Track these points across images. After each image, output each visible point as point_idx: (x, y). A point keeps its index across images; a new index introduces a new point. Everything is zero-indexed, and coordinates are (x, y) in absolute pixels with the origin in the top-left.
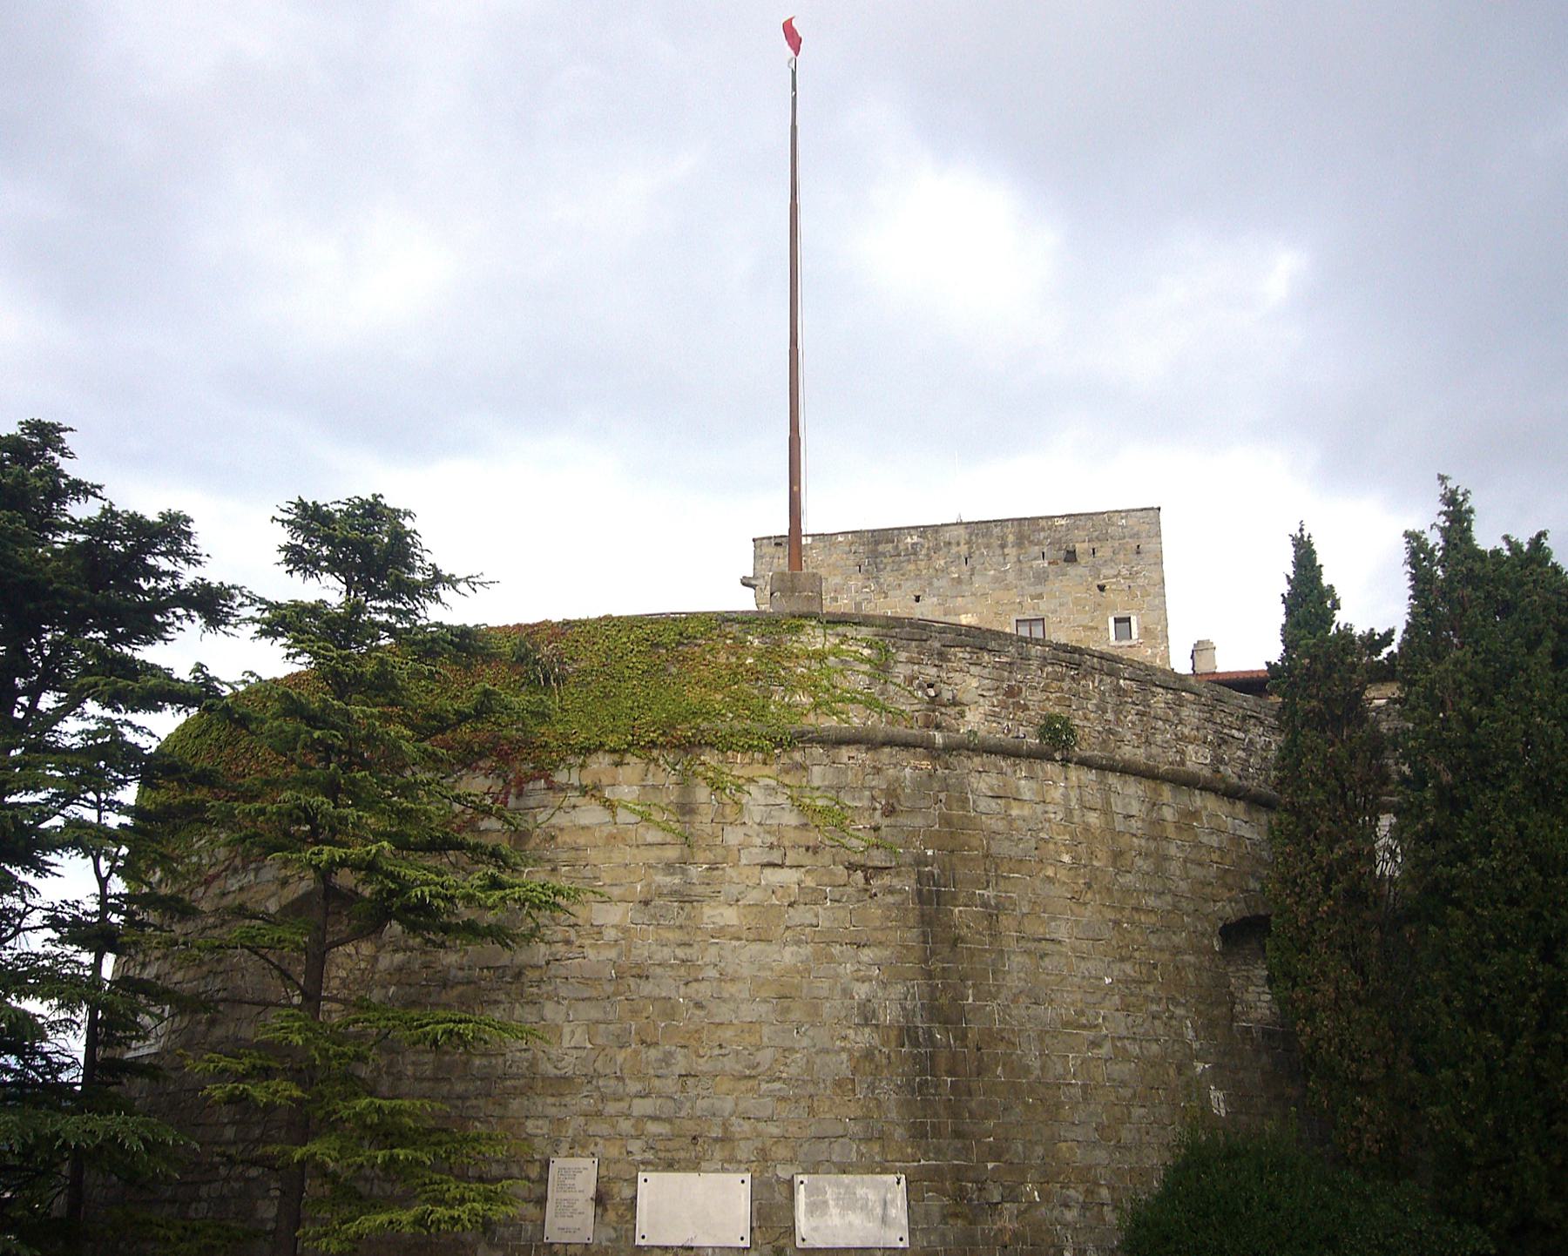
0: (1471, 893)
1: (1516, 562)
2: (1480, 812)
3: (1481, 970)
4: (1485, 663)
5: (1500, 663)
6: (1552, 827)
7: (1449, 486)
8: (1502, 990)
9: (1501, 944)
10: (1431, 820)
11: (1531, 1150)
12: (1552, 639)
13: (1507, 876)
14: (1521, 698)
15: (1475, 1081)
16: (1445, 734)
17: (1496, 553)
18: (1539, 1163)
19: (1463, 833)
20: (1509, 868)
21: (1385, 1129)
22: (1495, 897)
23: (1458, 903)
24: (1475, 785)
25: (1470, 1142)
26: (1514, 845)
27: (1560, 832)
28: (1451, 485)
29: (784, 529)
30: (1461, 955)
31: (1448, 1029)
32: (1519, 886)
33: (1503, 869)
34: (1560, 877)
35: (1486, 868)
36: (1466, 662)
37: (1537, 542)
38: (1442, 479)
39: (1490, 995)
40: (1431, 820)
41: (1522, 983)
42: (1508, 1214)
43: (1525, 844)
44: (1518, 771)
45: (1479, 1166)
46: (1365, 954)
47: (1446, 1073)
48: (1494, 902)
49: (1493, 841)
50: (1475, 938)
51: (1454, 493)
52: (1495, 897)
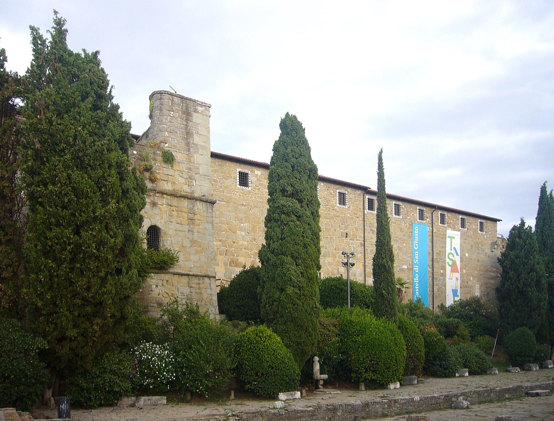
0: (46, 201)
1: (85, 61)
2: (53, 165)
3: (49, 234)
4: (62, 99)
5: (69, 101)
6: (83, 178)
7: (58, 16)
8: (57, 244)
9: (58, 225)
10: (30, 164)
11: (65, 309)
12: (93, 97)
13: (62, 196)
14: (75, 118)
15: (44, 280)
16: (39, 126)
17: (78, 55)
18: (68, 314)
19: (44, 173)
20: (63, 192)
21: (12, 298)
22: (57, 204)
23: (41, 204)
24: (52, 153)
25: (40, 304)
26: (65, 182)
27: (86, 181)
28: (59, 16)
30: (41, 226)
31: (34, 257)
32: (66, 201)
33: (60, 192)
34: (84, 200)
35: (53, 190)
36: (51, 95)
37: (96, 54)
38: (56, 12)
39: (52, 245)
40: (30, 164)
41: (65, 242)
42: (55, 333)
43: (70, 183)
44: (70, 150)
45: (45, 314)
46: (6, 223)
47: (33, 276)
48: (56, 206)
49: (57, 179)
50: (47, 220)
51: (60, 20)
52: (57, 204)
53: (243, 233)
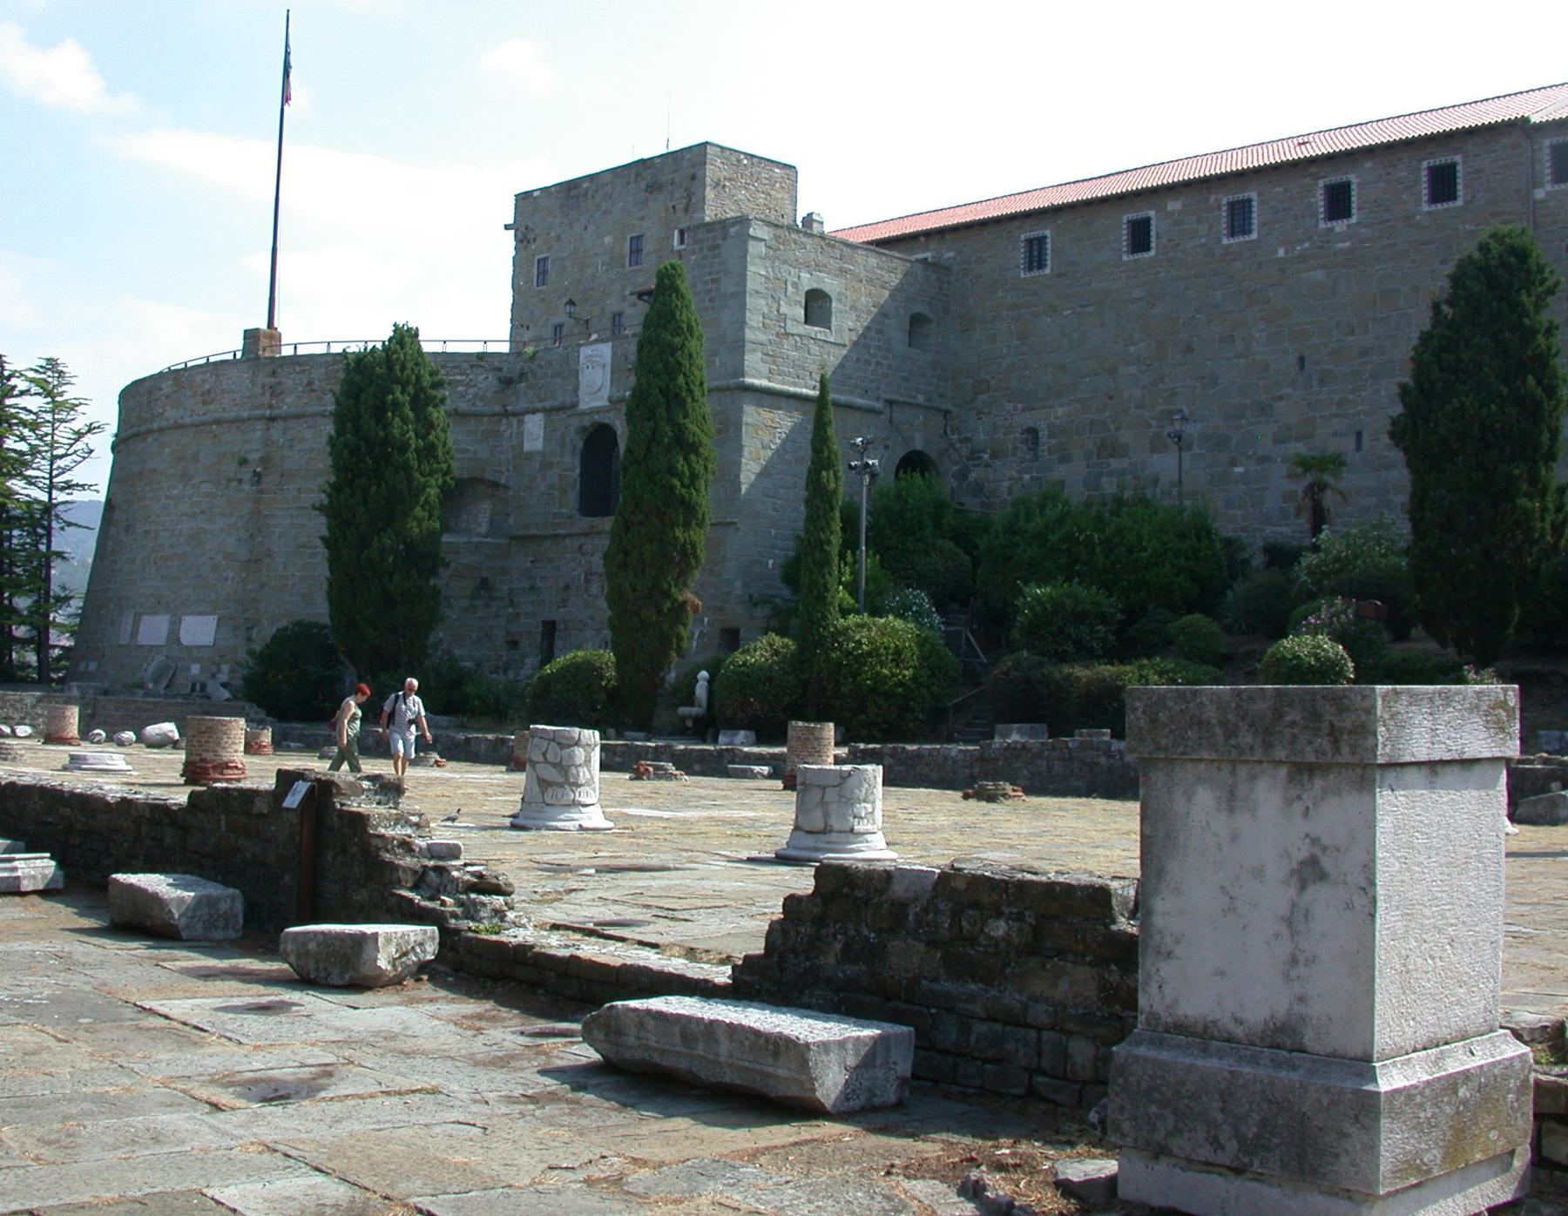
29: (263, 325)
53: (1133, 369)
